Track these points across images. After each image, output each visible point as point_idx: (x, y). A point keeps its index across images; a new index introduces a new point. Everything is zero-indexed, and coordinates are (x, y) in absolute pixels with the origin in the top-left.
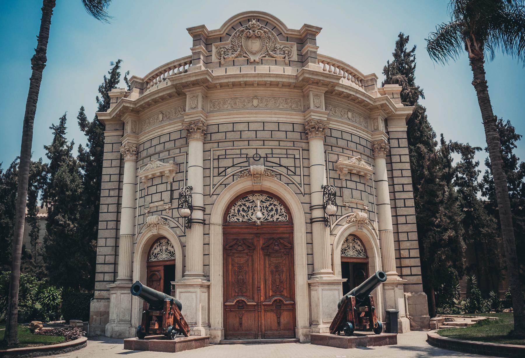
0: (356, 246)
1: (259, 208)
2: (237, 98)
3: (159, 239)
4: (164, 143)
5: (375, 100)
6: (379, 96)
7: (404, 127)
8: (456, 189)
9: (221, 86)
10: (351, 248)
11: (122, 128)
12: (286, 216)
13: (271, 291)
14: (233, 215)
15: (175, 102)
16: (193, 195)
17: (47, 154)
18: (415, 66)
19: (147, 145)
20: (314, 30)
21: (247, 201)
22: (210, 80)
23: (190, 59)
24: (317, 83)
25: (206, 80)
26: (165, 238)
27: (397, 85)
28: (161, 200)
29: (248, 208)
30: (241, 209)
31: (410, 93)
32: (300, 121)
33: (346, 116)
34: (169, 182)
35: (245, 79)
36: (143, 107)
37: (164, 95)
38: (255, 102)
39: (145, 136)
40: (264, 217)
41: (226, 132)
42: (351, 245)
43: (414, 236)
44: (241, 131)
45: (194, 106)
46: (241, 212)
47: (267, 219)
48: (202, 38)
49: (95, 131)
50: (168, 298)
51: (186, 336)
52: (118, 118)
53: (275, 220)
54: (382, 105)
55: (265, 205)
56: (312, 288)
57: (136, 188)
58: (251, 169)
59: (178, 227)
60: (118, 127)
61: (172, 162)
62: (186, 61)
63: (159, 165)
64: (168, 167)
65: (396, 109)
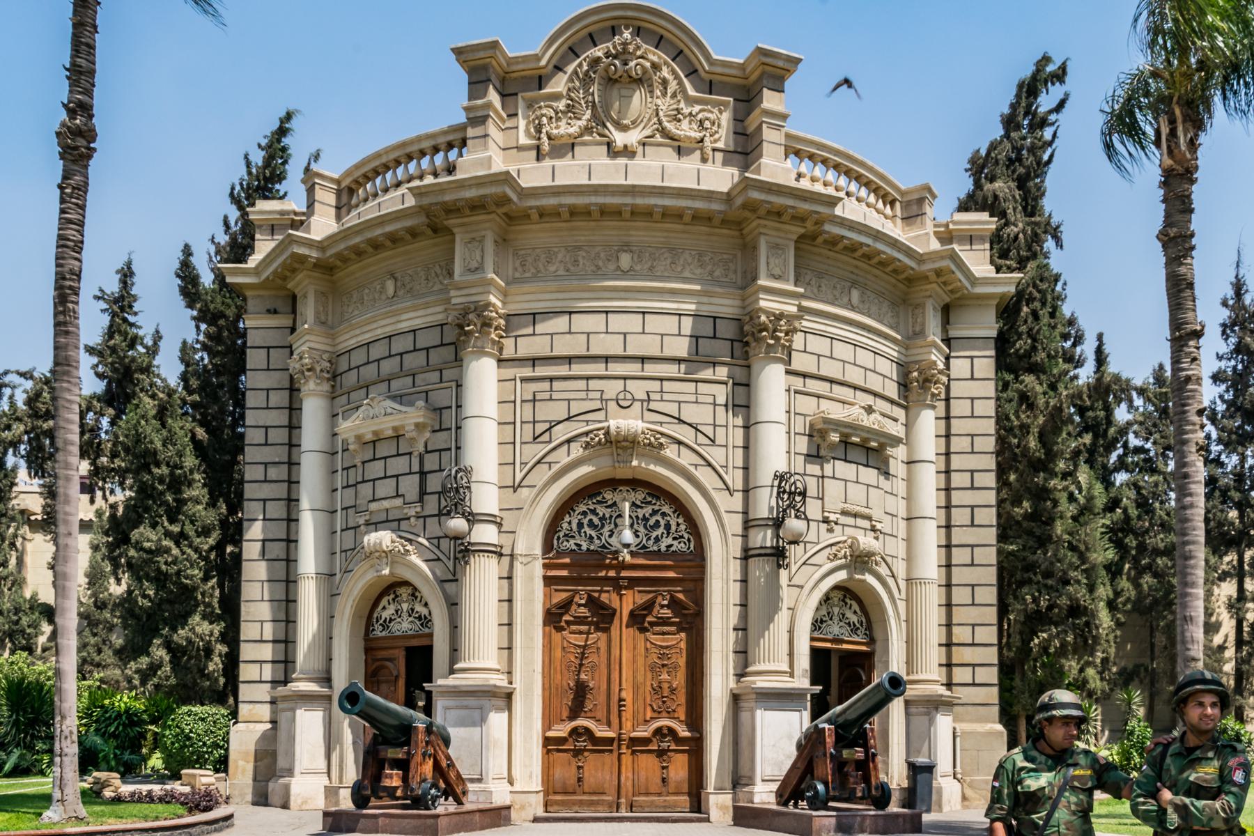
0: (849, 614)
1: (627, 521)
2: (579, 248)
3: (392, 588)
4: (401, 354)
5: (920, 259)
6: (935, 245)
7: (992, 328)
8: (1121, 478)
9: (541, 215)
10: (836, 619)
11: (289, 309)
12: (689, 540)
13: (649, 709)
14: (566, 535)
15: (425, 249)
16: (473, 486)
17: (95, 367)
18: (1051, 156)
19: (358, 358)
20: (780, 64)
21: (599, 502)
22: (514, 197)
23: (459, 136)
24: (777, 213)
25: (506, 200)
26: (406, 583)
27: (985, 216)
28: (398, 496)
29: (603, 519)
30: (586, 521)
31: (1021, 235)
32: (730, 310)
33: (846, 300)
34: (416, 454)
35: (601, 200)
36: (343, 258)
37: (397, 231)
38: (625, 260)
39: (352, 333)
40: (638, 540)
41: (552, 335)
42: (836, 610)
43: (989, 595)
44: (588, 334)
45: (474, 265)
46: (586, 529)
47: (644, 547)
48: (493, 77)
49: (218, 311)
50: (419, 720)
51: (460, 803)
52: (279, 281)
53: (663, 548)
54: (939, 273)
55: (640, 513)
56: (743, 704)
57: (333, 463)
58: (613, 429)
59: (439, 559)
60: (279, 305)
61: (421, 403)
62: (450, 138)
63: (389, 410)
64: (412, 416)
65: (974, 281)
